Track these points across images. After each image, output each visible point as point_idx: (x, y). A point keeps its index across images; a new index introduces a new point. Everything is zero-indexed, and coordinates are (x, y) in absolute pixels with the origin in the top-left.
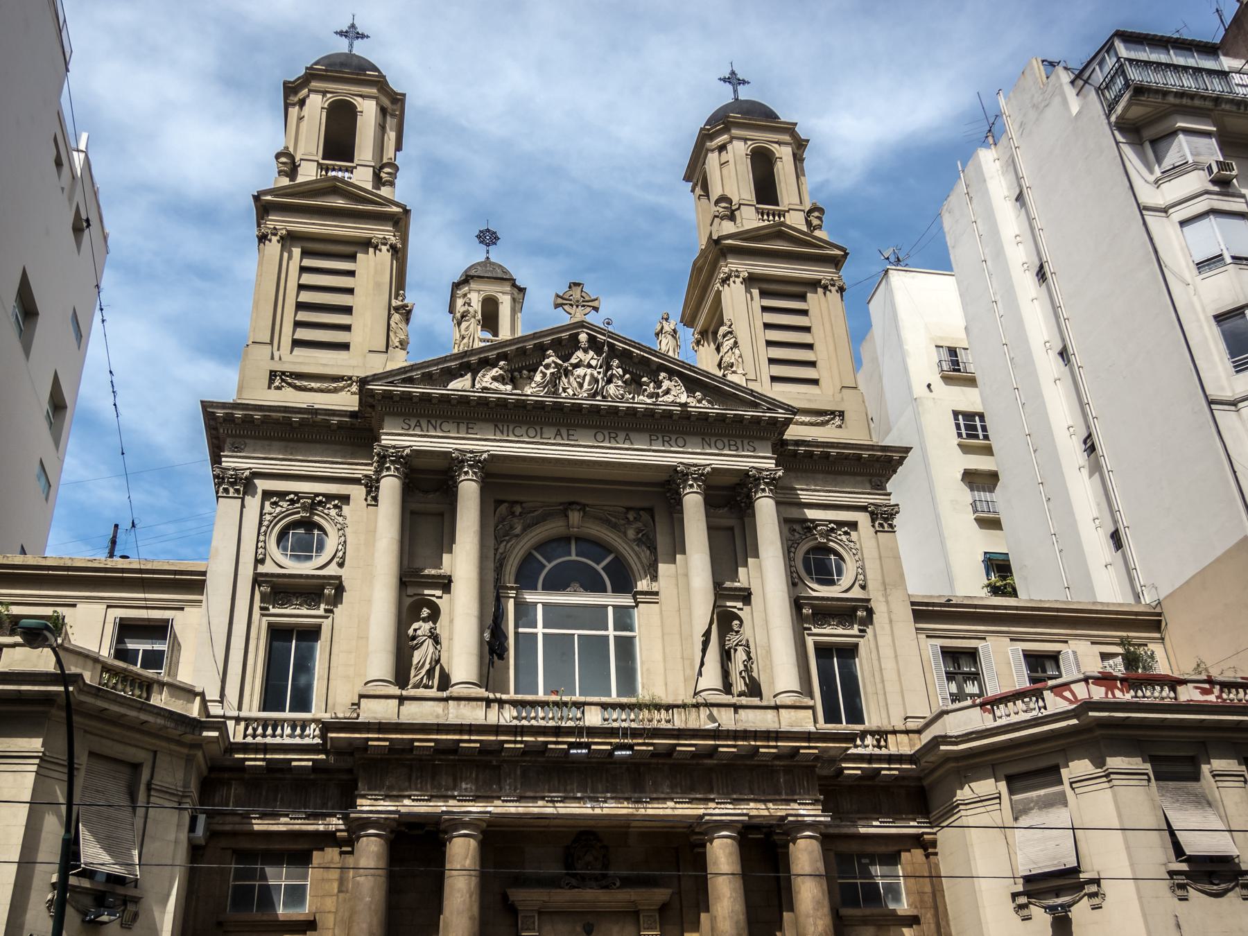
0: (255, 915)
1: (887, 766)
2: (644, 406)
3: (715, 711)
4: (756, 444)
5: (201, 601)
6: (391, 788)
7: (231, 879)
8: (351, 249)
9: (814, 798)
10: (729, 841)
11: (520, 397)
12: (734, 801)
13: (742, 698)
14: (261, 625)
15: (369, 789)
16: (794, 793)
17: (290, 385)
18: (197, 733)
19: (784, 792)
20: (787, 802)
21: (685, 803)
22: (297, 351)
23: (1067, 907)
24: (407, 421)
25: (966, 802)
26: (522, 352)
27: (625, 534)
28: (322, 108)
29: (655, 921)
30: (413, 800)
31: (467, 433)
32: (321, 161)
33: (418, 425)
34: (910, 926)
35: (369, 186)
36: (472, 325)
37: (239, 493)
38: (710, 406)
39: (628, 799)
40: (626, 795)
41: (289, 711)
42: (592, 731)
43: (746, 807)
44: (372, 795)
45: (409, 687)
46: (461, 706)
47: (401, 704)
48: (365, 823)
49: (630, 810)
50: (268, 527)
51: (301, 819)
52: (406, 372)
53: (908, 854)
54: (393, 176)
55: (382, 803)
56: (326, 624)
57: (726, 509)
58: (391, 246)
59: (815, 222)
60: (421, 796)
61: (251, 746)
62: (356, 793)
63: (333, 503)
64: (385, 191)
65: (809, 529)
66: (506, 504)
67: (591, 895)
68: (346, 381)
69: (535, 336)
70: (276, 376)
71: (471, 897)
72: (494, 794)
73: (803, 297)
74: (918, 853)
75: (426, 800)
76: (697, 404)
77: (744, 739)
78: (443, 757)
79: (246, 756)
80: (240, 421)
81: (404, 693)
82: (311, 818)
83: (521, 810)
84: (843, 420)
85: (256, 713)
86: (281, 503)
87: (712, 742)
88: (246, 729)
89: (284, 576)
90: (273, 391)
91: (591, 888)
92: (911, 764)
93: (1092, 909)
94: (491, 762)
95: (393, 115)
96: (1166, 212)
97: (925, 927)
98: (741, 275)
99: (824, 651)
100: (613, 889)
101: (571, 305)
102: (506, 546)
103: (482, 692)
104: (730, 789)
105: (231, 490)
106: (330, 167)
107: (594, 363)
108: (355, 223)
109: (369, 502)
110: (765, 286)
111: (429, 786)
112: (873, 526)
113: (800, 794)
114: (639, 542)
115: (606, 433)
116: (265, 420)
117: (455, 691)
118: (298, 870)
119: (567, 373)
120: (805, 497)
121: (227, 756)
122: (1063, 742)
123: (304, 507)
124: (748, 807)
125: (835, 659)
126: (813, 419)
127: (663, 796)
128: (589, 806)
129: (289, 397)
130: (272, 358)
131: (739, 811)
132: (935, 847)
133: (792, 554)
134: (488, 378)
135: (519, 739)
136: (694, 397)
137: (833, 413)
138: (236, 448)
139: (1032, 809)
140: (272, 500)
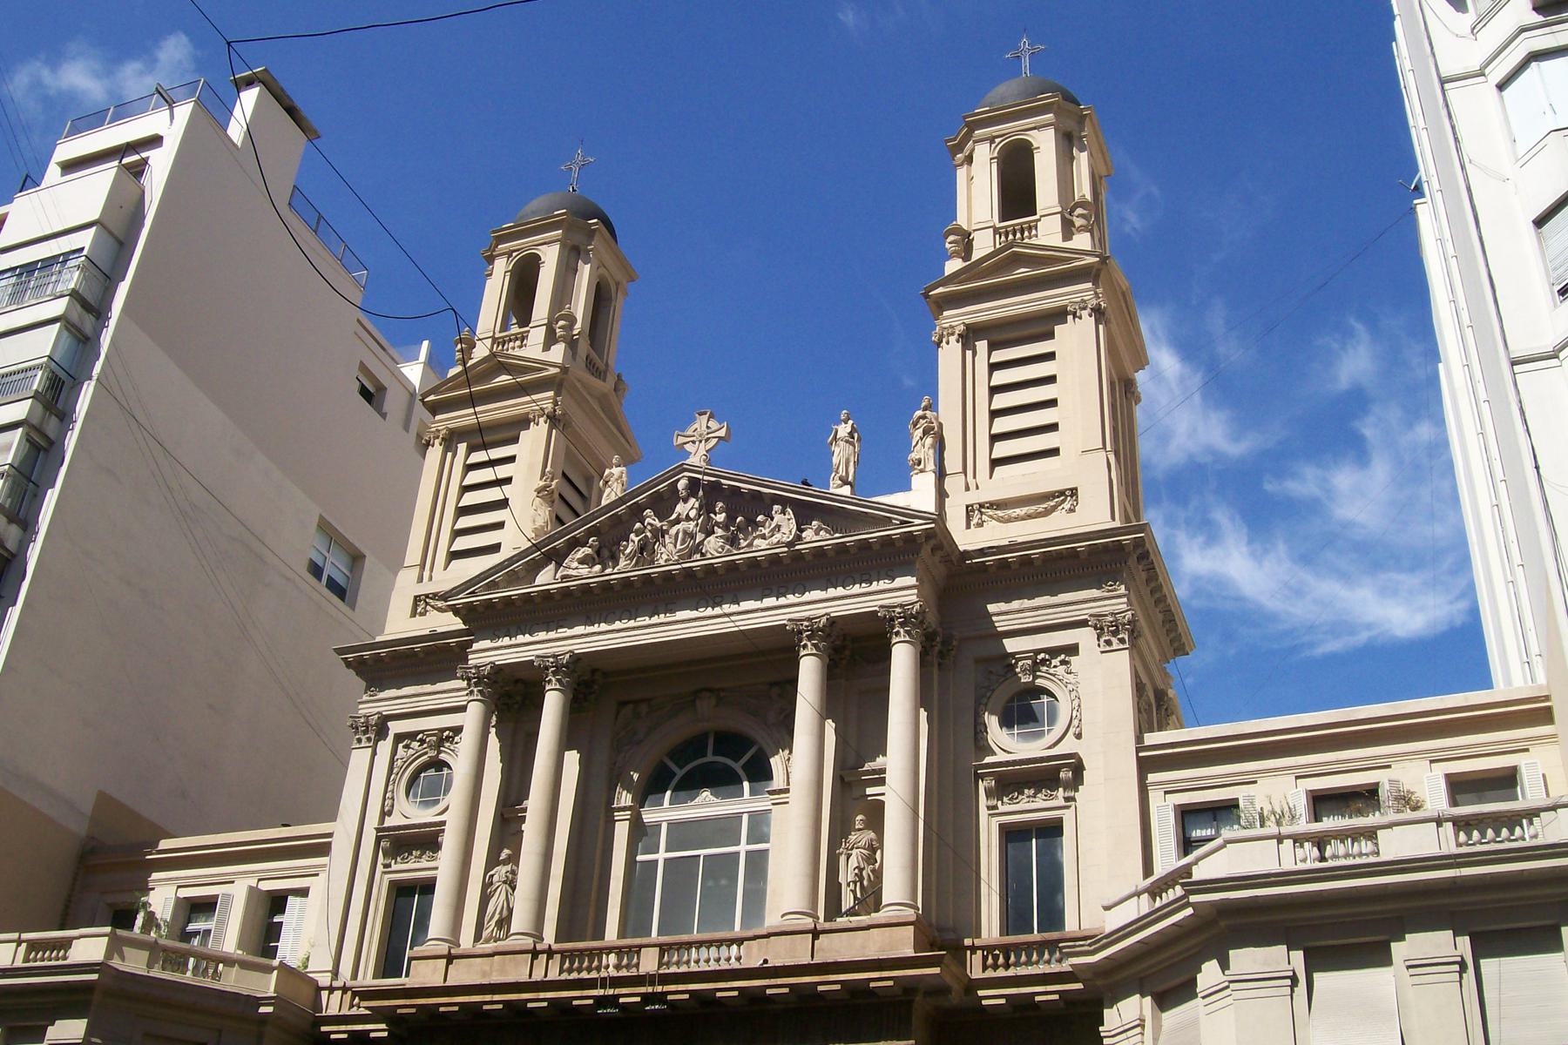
8: (1042, 325)
25: (1113, 1033)
38: (828, 536)
47: (449, 962)
56: (1068, 817)
66: (631, 706)
68: (1058, 497)
70: (973, 511)
76: (815, 536)
84: (1077, 500)
88: (985, 958)
89: (1014, 763)
96: (1483, 75)
101: (694, 442)
105: (1114, 640)
119: (664, 533)
122: (1193, 942)
126: (1041, 507)
130: (967, 489)
137: (1062, 493)
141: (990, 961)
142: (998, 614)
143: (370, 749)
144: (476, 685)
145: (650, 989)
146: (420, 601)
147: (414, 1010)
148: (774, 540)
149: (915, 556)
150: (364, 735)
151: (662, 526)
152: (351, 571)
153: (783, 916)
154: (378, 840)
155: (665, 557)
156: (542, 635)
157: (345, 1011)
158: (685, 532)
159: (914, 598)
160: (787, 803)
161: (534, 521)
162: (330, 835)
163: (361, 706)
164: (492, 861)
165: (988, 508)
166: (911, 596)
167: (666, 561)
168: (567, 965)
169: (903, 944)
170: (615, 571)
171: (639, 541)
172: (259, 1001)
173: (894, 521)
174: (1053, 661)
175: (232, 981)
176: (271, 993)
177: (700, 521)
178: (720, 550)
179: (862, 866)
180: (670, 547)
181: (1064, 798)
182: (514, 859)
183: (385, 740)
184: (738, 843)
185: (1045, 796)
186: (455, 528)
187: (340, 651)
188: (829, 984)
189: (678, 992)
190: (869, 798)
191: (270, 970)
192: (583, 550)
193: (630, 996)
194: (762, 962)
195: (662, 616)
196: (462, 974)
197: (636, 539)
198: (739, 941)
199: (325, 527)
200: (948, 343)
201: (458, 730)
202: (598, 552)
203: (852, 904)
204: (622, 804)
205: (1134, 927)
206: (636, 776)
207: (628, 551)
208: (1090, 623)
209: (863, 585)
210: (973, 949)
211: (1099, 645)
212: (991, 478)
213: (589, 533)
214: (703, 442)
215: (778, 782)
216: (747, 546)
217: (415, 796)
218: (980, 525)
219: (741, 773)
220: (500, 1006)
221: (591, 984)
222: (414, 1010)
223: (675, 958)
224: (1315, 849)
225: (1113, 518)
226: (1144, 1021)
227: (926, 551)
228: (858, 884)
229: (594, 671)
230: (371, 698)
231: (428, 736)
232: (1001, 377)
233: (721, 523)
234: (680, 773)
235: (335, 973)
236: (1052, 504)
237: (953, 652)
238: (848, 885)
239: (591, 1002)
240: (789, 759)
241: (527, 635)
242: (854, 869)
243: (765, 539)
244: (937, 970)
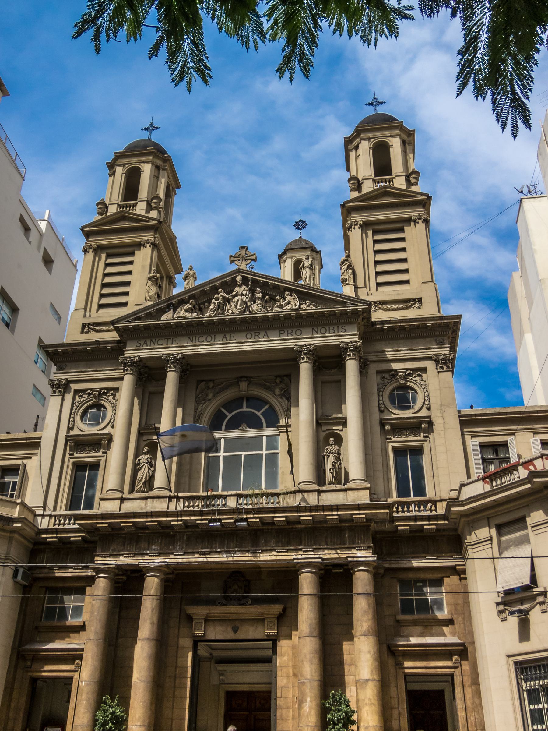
0: (56, 623)
1: (428, 523)
2: (273, 314)
3: (305, 494)
4: (347, 327)
5: (37, 453)
6: (114, 550)
9: (367, 545)
10: (310, 574)
11: (199, 319)
12: (314, 550)
13: (331, 485)
14: (69, 463)
15: (102, 552)
16: (354, 543)
17: (93, 330)
18: (11, 525)
19: (348, 542)
20: (350, 548)
21: (283, 552)
23: (527, 612)
24: (139, 342)
25: (472, 543)
26: (204, 292)
27: (274, 392)
28: (370, 148)
29: (274, 624)
30: (125, 557)
31: (172, 344)
32: (120, 203)
33: (146, 343)
34: (447, 626)
35: (404, 187)
36: (191, 281)
37: (61, 393)
38: (315, 308)
39: (248, 551)
40: (247, 549)
41: (83, 510)
42: (232, 511)
43: (322, 553)
44: (102, 555)
46: (155, 502)
48: (98, 571)
49: (250, 558)
50: (76, 409)
51: (79, 569)
52: (136, 314)
53: (448, 579)
54: (158, 204)
55: (108, 559)
56: (426, 445)
57: (336, 369)
58: (152, 244)
59: (413, 181)
60: (129, 554)
61: (49, 530)
62: (94, 554)
63: (417, 373)
64: (414, 188)
65: (394, 376)
66: (204, 382)
67: (233, 609)
68: (412, 301)
69: (210, 282)
70: (85, 326)
71: (152, 611)
72: (170, 552)
73: (402, 230)
74: (455, 579)
75: (132, 556)
76: (307, 308)
77: (317, 511)
78: (142, 531)
79: (48, 536)
80: (61, 353)
81: (321, 488)
82: (85, 569)
83: (185, 560)
84: (421, 303)
85: (64, 512)
86: (84, 396)
87: (296, 514)
88: (55, 521)
90: (84, 335)
91: (233, 605)
92: (444, 520)
93: (542, 613)
94: (170, 533)
95: (409, 144)
97: (456, 626)
98: (359, 224)
99: (399, 452)
100: (246, 605)
103: (316, 487)
104: (313, 542)
105: (445, 367)
106: (380, 181)
107: (244, 293)
108: (383, 212)
109: (439, 370)
110: (377, 227)
111: (134, 549)
112: (437, 369)
113: (358, 543)
114: (282, 395)
115: (327, 328)
116: (93, 350)
117: (351, 485)
118: (80, 597)
119: (229, 301)
120: (390, 356)
121: (38, 537)
123: (95, 397)
124: (324, 553)
125: (408, 456)
126: (400, 306)
127: (269, 548)
128: (225, 556)
129: (93, 337)
131: (318, 556)
132: (465, 574)
133: (381, 393)
134: (183, 311)
135: (179, 519)
136: (306, 304)
137: (414, 300)
138: (61, 368)
139: (511, 546)
140: (79, 394)
141: (57, 522)
154: (66, 442)
157: (51, 527)
167: (231, 313)
171: (218, 303)
178: (259, 310)
188: (126, 523)
194: (298, 503)
197: (216, 302)
200: (354, 228)
204: (281, 424)
205: (499, 490)
212: (377, 291)
213: (190, 297)
214: (244, 261)
216: (270, 310)
217: (86, 421)
232: (109, 270)
235: (44, 507)
236: (410, 304)
242: (332, 463)
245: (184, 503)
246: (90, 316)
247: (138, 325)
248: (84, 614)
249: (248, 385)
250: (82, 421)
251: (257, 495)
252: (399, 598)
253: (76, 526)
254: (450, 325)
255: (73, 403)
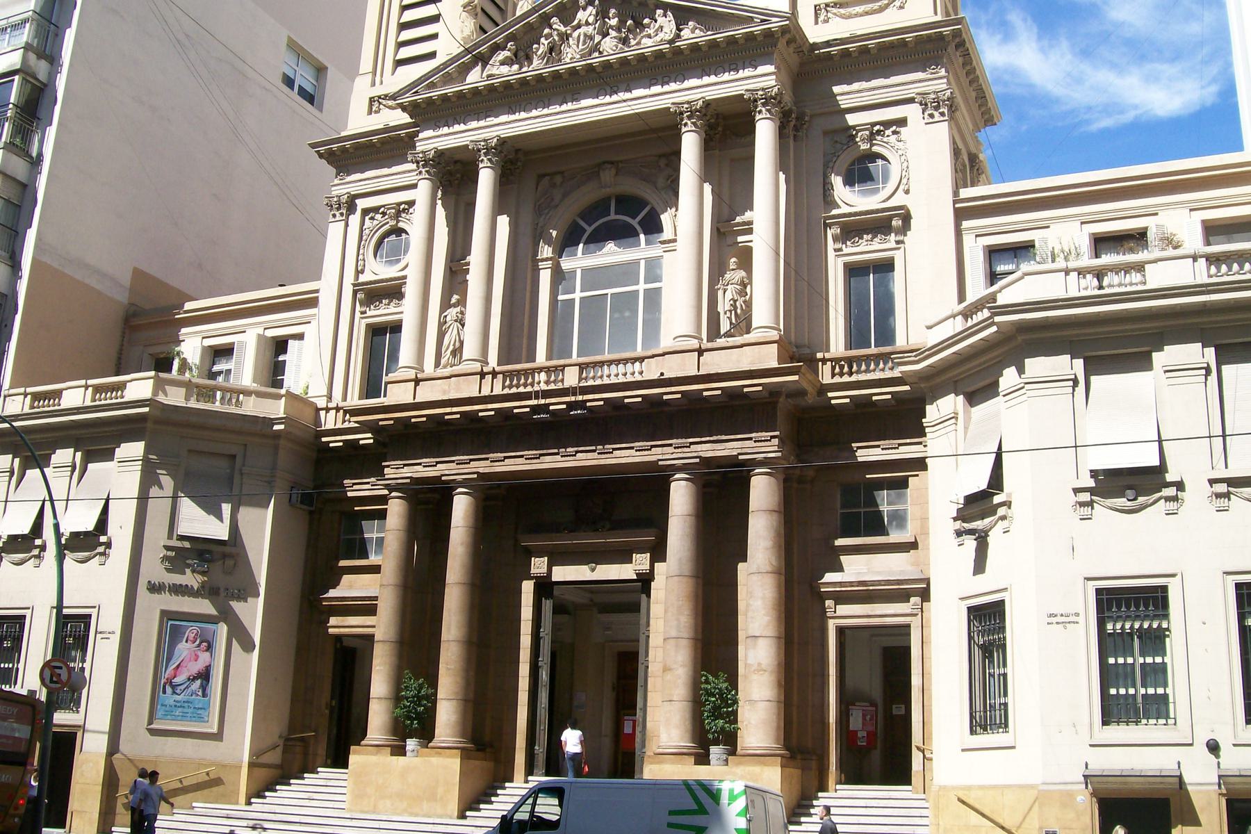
7: (839, 505)
10: (683, 483)
22: (401, 69)
38: (702, 34)
45: (440, 367)
70: (820, 10)
76: (692, 34)
88: (833, 368)
99: (854, 271)
102: (545, 219)
109: (926, 121)
141: (837, 370)
142: (842, 94)
143: (343, 222)
144: (424, 166)
145: (573, 399)
146: (374, 101)
147: (392, 422)
148: (658, 38)
149: (774, 48)
150: (338, 211)
151: (566, 31)
152: (317, 81)
153: (674, 339)
154: (355, 293)
155: (570, 56)
156: (474, 124)
157: (339, 425)
158: (585, 35)
159: (773, 83)
160: (675, 250)
161: (462, 31)
162: (317, 291)
163: (333, 189)
164: (445, 305)
165: (832, 7)
166: (771, 81)
167: (571, 59)
168: (508, 382)
169: (769, 358)
170: (530, 69)
172: (271, 422)
173: (755, 20)
174: (886, 131)
175: (251, 407)
176: (282, 415)
177: (597, 25)
178: (614, 48)
179: (736, 299)
180: (575, 47)
181: (896, 241)
182: (462, 302)
183: (354, 214)
184: (638, 284)
185: (881, 240)
186: (398, 40)
187: (313, 146)
188: (712, 390)
189: (595, 400)
190: (740, 245)
191: (279, 397)
192: (503, 53)
193: (557, 403)
194: (659, 375)
195: (570, 104)
196: (427, 393)
198: (641, 359)
199: (293, 46)
201: (411, 203)
202: (516, 55)
203: (728, 329)
204: (545, 256)
206: (554, 233)
207: (539, 53)
208: (916, 100)
209: (732, 73)
210: (824, 361)
211: (924, 118)
213: (510, 38)
215: (667, 234)
217: (381, 257)
218: (826, 21)
219: (638, 228)
220: (458, 416)
221: (527, 396)
222: (392, 422)
223: (592, 374)
224: (933, 412)
225: (936, 13)
226: (957, 414)
227: (782, 44)
228: (733, 312)
229: (517, 151)
230: (341, 181)
231: (388, 209)
233: (614, 26)
234: (589, 230)
237: (805, 126)
238: (725, 313)
239: (528, 410)
240: (675, 216)
241: (462, 125)
243: (650, 38)
244: (796, 378)
245: (504, 382)
246: (382, 83)
247: (493, 84)
248: (910, 525)
249: (617, 174)
250: (375, 256)
251: (626, 361)
252: (375, 537)
253: (353, 425)
254: (946, 37)
255: (361, 231)
